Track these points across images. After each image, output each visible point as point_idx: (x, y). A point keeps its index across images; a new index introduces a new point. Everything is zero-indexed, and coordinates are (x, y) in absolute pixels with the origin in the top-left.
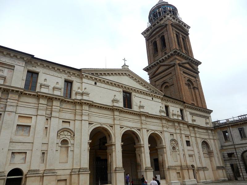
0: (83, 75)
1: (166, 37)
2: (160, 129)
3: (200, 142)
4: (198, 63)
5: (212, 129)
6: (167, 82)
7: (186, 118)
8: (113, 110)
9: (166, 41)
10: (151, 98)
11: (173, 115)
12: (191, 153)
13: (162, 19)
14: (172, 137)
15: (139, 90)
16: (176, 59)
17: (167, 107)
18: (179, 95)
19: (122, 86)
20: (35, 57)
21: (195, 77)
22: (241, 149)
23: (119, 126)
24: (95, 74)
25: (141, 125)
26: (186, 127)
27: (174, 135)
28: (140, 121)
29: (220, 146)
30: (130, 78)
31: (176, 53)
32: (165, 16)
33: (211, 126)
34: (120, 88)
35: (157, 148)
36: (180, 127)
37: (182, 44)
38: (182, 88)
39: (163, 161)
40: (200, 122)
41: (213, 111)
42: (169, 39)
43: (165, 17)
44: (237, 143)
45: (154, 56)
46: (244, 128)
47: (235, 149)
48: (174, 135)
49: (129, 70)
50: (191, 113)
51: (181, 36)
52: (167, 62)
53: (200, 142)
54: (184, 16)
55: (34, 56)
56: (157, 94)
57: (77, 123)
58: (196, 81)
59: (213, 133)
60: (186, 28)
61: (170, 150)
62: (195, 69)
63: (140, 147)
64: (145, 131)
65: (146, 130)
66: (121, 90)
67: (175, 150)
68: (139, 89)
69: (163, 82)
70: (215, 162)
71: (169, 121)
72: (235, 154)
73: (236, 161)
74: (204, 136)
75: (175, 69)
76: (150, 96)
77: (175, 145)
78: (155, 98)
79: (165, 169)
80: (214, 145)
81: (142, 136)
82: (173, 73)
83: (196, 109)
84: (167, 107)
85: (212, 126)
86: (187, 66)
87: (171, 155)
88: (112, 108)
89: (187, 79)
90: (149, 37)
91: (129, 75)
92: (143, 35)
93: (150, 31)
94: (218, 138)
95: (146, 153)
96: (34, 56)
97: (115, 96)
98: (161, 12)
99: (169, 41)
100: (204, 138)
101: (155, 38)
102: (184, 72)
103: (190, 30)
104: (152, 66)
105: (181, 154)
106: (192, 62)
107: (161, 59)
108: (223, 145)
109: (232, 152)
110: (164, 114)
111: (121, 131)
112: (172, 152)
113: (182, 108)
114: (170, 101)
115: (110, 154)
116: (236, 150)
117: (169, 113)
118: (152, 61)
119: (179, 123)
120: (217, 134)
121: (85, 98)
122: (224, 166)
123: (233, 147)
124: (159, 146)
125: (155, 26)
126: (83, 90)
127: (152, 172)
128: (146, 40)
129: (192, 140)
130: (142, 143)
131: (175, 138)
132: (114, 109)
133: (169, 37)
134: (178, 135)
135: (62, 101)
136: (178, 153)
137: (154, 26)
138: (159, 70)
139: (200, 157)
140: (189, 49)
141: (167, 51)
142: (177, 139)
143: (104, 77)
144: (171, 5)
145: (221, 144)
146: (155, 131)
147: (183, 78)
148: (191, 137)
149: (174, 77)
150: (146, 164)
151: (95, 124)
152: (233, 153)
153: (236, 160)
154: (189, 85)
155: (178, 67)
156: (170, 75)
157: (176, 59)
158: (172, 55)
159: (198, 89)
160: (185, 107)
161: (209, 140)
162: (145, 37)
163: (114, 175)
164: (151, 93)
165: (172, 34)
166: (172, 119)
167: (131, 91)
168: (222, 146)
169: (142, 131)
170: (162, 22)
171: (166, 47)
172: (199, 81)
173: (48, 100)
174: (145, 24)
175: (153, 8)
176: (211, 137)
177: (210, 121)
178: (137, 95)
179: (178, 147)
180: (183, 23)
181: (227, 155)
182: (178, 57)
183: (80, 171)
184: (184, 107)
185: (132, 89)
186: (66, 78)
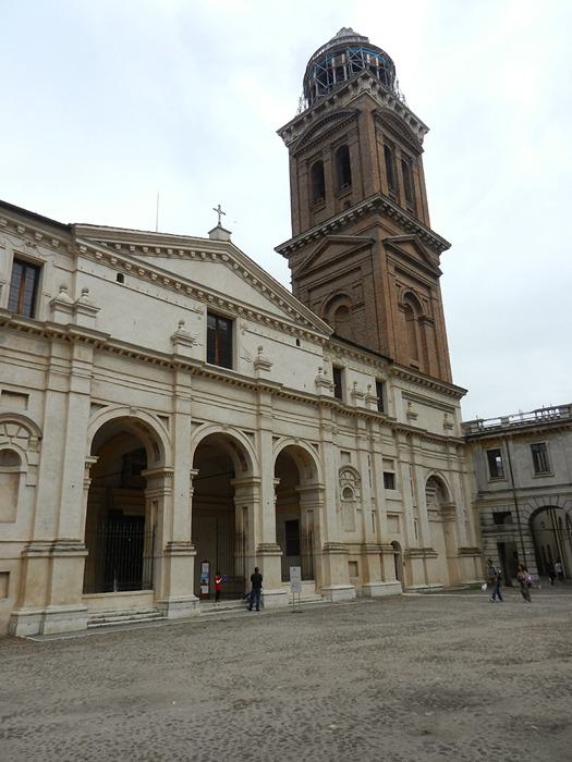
0: (78, 245)
8: (172, 367)
10: (293, 341)
11: (356, 395)
12: (395, 508)
19: (206, 295)
22: (531, 502)
24: (119, 247)
28: (255, 408)
44: (522, 486)
51: (398, 155)
57: (53, 400)
58: (431, 298)
60: (416, 131)
66: (203, 307)
72: (514, 514)
73: (514, 536)
77: (352, 483)
79: (315, 552)
85: (461, 435)
86: (409, 250)
88: (169, 360)
97: (182, 323)
103: (426, 137)
113: (382, 376)
121: (82, 320)
123: (510, 495)
126: (78, 295)
127: (279, 558)
131: (354, 464)
133: (363, 152)
138: (325, 258)
143: (149, 260)
151: (282, 438)
153: (514, 530)
157: (377, 225)
159: (433, 323)
160: (392, 374)
163: (161, 564)
165: (373, 144)
167: (234, 314)
168: (481, 493)
176: (455, 466)
178: (252, 326)
179: (360, 489)
181: (491, 516)
183: (55, 549)
185: (236, 307)
186: (21, 250)
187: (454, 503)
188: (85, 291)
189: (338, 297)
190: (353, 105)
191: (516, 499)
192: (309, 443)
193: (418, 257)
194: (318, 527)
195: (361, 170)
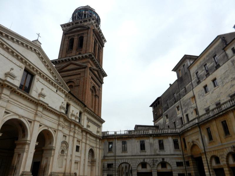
1: (85, 39)
2: (55, 126)
3: (88, 149)
4: (105, 75)
6: (73, 82)
7: (82, 121)
9: (84, 42)
10: (55, 90)
11: (72, 115)
12: (78, 159)
13: (86, 21)
14: (64, 139)
15: (46, 75)
16: (89, 62)
17: (68, 105)
18: (81, 97)
19: (26, 62)
21: (99, 86)
22: (120, 161)
23: (4, 110)
25: (35, 117)
26: (80, 131)
28: (35, 111)
29: (103, 156)
30: (39, 57)
31: (91, 57)
32: (90, 19)
33: (100, 135)
34: (22, 62)
35: (45, 148)
36: (75, 129)
37: (97, 52)
38: (87, 91)
39: (47, 166)
40: (93, 129)
42: (88, 41)
43: (90, 20)
44: (118, 155)
45: (67, 52)
48: (67, 137)
49: (40, 48)
50: (88, 119)
51: (98, 45)
52: (79, 62)
53: (88, 149)
54: (105, 28)
56: (63, 88)
58: (99, 90)
59: (101, 142)
60: (103, 41)
61: (59, 153)
62: (101, 79)
63: (25, 143)
64: (37, 124)
65: (39, 124)
66: (23, 66)
67: (63, 154)
68: (46, 75)
69: (68, 80)
70: (95, 171)
71: (66, 120)
72: (114, 165)
74: (92, 143)
75: (86, 71)
76: (55, 87)
77: (65, 148)
78: (60, 91)
80: (98, 155)
81: (31, 129)
82: (82, 75)
83: (93, 116)
84: (68, 105)
85: (101, 136)
86: (96, 73)
87: (58, 159)
89: (93, 85)
90: (69, 31)
91: (39, 54)
92: (62, 27)
93: (71, 26)
94: (103, 148)
95: (29, 153)
98: (87, 15)
99: (87, 43)
100: (92, 145)
101: (74, 36)
102: (92, 78)
104: (62, 61)
105: (68, 159)
106: (101, 73)
107: (74, 57)
108: (106, 155)
109: (112, 163)
110: (63, 111)
111: (5, 117)
112: (59, 155)
113: (82, 111)
114: (73, 100)
117: (33, 79)
118: (63, 56)
119: (75, 125)
120: (103, 143)
123: (114, 158)
124: (47, 146)
125: (77, 25)
128: (63, 33)
129: (82, 146)
130: (29, 138)
131: (67, 140)
132: (5, 85)
133: (88, 40)
134: (71, 138)
137: (76, 23)
138: (68, 68)
139: (84, 165)
140: (101, 60)
141: (82, 52)
142: (69, 142)
144: (96, 14)
145: (104, 154)
146: (48, 128)
147: (90, 83)
149: (82, 79)
150: (24, 168)
152: (112, 164)
153: (113, 170)
154: (92, 92)
155: (89, 71)
156: (79, 76)
157: (89, 62)
158: (86, 57)
160: (85, 111)
162: (63, 30)
164: (58, 84)
165: (92, 38)
166: (70, 119)
167: (35, 73)
168: (104, 157)
169: (34, 124)
170: (85, 24)
171: (82, 48)
172: (101, 91)
174: (67, 19)
175: (80, 7)
176: (98, 146)
177: (100, 130)
178: (41, 80)
179: (68, 151)
180: (102, 35)
181: (106, 165)
182: (91, 62)
184: (84, 111)
185: (37, 71)
190: (88, 26)
191: (115, 159)
192: (53, 129)
194: (49, 165)
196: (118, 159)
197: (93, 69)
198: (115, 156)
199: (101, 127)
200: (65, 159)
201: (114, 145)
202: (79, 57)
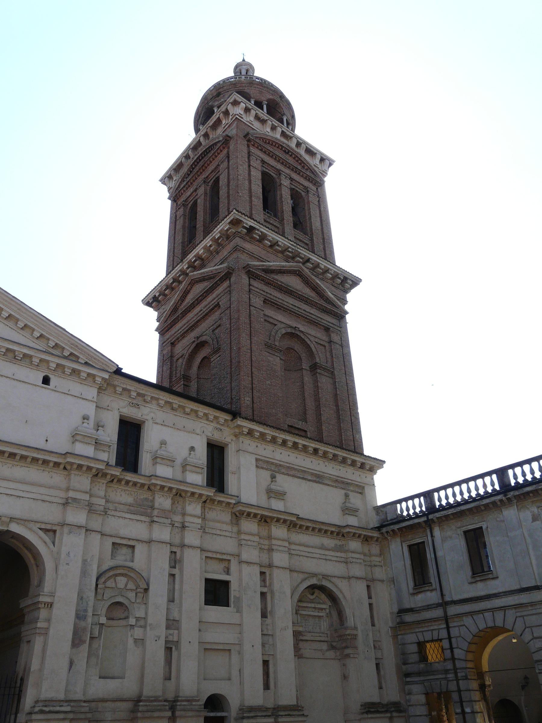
1: (223, 182)
5: (372, 538)
20: (122, 371)
21: (327, 329)
22: (468, 621)
27: (232, 561)
41: (384, 462)
44: (456, 598)
46: (484, 527)
47: (447, 623)
48: (140, 549)
51: (286, 182)
53: (288, 592)
55: (122, 369)
58: (330, 342)
60: (314, 162)
86: (294, 282)
96: (122, 369)
99: (228, 192)
103: (331, 171)
108: (407, 605)
115: (29, 642)
116: (448, 628)
122: (402, 702)
123: (438, 613)
135: (112, 481)
136: (138, 633)
138: (190, 299)
148: (240, 562)
159: (332, 373)
161: (345, 582)
168: (402, 611)
173: (109, 485)
176: (357, 570)
182: (248, 246)
187: (356, 628)
188: (163, 443)
189: (200, 345)
191: (446, 619)
192: (35, 527)
193: (307, 292)
195: (228, 196)
196: (459, 616)
197: (264, 270)
198: (444, 604)
199: (367, 490)
200: (136, 641)
201: (433, 556)
202: (206, 246)
